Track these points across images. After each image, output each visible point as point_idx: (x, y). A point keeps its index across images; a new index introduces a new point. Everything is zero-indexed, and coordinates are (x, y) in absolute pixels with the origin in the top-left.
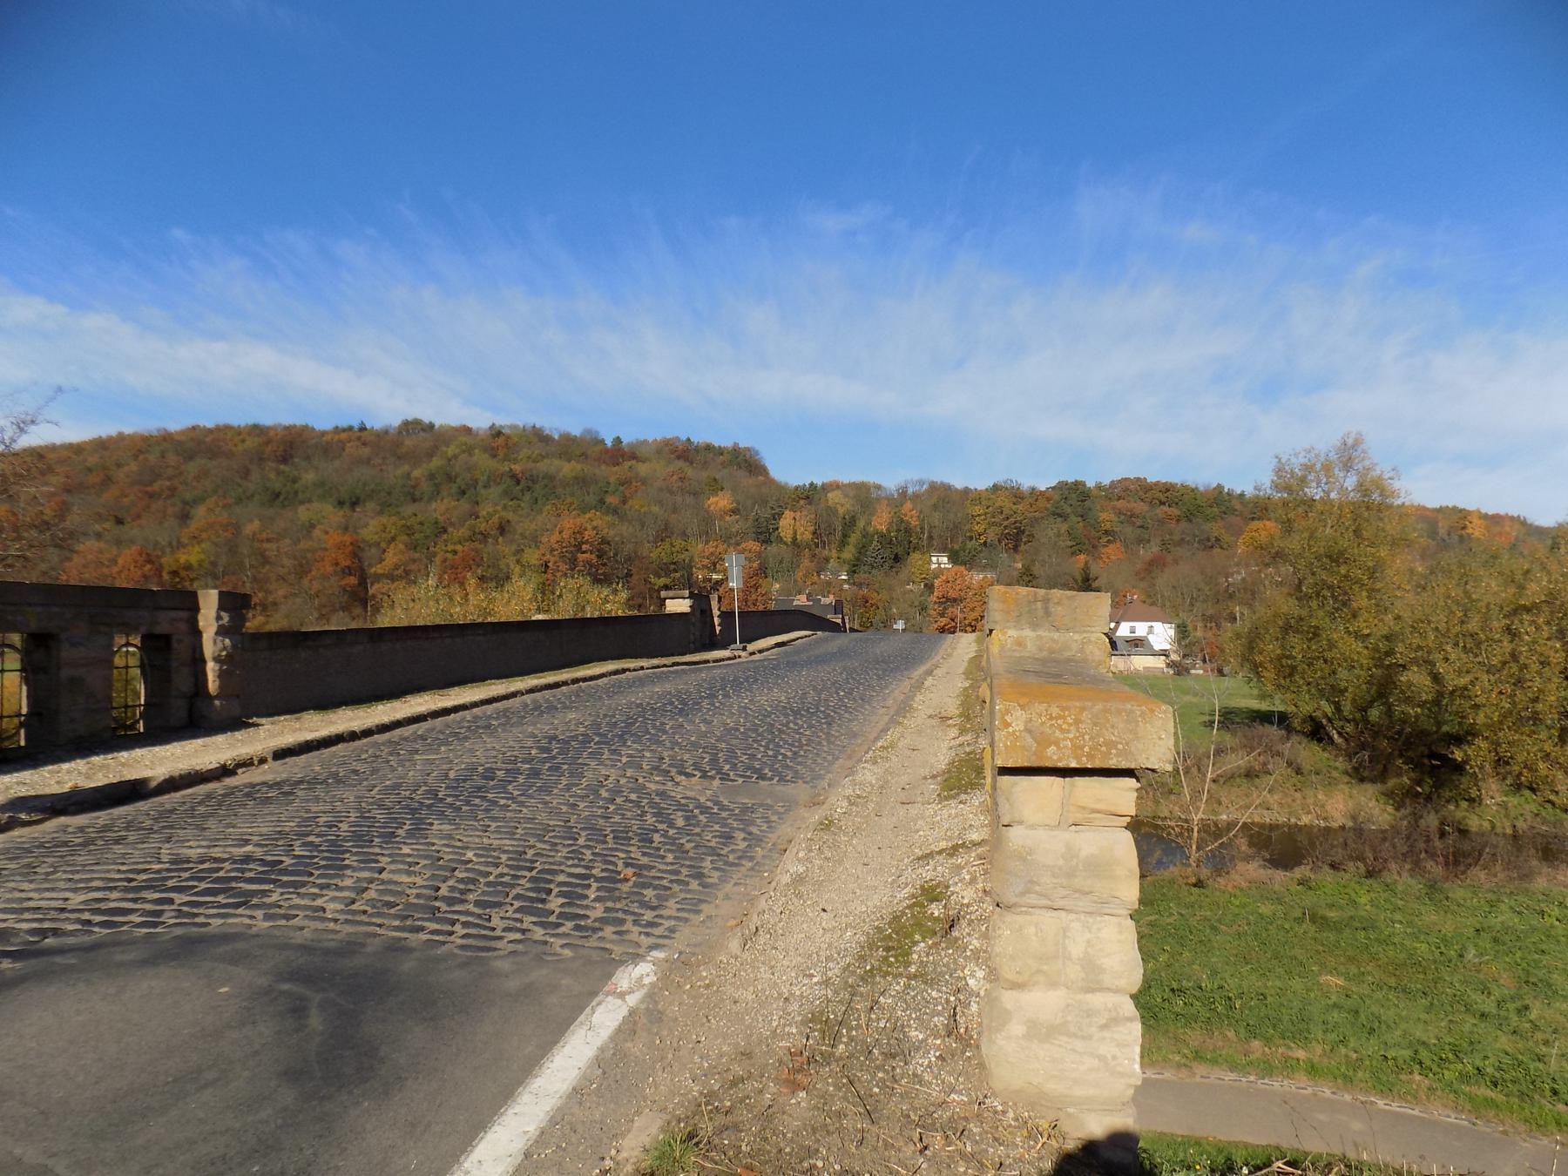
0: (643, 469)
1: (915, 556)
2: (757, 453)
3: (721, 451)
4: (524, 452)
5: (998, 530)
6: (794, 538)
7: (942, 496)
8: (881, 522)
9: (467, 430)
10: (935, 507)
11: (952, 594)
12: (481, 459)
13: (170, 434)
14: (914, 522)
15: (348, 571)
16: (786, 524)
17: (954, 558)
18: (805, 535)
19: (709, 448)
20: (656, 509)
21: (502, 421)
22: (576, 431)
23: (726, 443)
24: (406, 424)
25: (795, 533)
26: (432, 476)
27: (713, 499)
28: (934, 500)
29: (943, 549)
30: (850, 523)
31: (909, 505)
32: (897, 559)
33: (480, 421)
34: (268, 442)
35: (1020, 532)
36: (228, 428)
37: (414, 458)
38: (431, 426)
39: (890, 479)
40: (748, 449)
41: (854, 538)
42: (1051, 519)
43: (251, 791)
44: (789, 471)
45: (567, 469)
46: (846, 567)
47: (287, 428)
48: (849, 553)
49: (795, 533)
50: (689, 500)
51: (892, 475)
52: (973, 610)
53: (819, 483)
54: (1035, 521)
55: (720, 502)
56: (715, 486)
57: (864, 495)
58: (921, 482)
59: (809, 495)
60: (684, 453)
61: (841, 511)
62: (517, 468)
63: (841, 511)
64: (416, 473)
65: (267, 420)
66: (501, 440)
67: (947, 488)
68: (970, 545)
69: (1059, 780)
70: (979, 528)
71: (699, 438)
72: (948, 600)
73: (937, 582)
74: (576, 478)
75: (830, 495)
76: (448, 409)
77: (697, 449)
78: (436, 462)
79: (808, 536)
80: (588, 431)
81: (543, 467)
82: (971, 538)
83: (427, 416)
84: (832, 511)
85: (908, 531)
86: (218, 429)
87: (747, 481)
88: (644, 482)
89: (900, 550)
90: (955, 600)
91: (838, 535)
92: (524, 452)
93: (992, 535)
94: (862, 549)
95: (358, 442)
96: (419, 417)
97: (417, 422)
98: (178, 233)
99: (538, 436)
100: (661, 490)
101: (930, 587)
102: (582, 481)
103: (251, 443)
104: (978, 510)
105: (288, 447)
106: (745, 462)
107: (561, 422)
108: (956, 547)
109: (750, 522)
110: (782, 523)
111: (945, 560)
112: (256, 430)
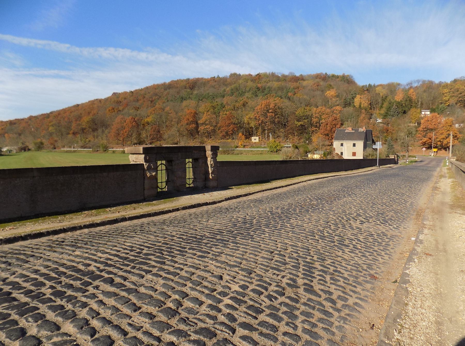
0: (305, 83)
1: (413, 110)
2: (352, 77)
3: (338, 77)
4: (264, 80)
5: (456, 99)
6: (360, 106)
7: (429, 86)
8: (399, 97)
10: (425, 91)
12: (250, 84)
14: (414, 97)
15: (192, 122)
16: (357, 101)
17: (433, 111)
18: (365, 104)
19: (333, 76)
20: (305, 97)
22: (286, 73)
25: (361, 103)
27: (328, 92)
28: (425, 88)
29: (428, 108)
30: (384, 99)
31: (412, 90)
32: (405, 112)
34: (188, 83)
39: (403, 80)
40: (348, 76)
41: (386, 105)
43: (220, 211)
44: (361, 81)
45: (275, 84)
46: (382, 117)
48: (383, 111)
49: (361, 103)
52: (442, 134)
53: (373, 84)
55: (330, 93)
56: (330, 87)
58: (418, 81)
59: (369, 89)
60: (325, 78)
61: (381, 94)
62: (259, 85)
63: (381, 94)
67: (431, 82)
68: (441, 106)
70: (446, 98)
71: (330, 73)
72: (428, 129)
73: (422, 121)
75: (377, 89)
77: (329, 77)
79: (366, 105)
80: (291, 73)
81: (268, 85)
82: (442, 103)
85: (410, 100)
86: (178, 80)
88: (304, 87)
89: (406, 109)
90: (432, 130)
91: (380, 105)
92: (264, 80)
93: (453, 101)
94: (389, 109)
95: (218, 82)
96: (393, 82)
101: (419, 124)
102: (281, 89)
103: (185, 83)
104: (446, 90)
105: (193, 85)
106: (347, 80)
108: (434, 107)
110: (356, 100)
111: (428, 113)
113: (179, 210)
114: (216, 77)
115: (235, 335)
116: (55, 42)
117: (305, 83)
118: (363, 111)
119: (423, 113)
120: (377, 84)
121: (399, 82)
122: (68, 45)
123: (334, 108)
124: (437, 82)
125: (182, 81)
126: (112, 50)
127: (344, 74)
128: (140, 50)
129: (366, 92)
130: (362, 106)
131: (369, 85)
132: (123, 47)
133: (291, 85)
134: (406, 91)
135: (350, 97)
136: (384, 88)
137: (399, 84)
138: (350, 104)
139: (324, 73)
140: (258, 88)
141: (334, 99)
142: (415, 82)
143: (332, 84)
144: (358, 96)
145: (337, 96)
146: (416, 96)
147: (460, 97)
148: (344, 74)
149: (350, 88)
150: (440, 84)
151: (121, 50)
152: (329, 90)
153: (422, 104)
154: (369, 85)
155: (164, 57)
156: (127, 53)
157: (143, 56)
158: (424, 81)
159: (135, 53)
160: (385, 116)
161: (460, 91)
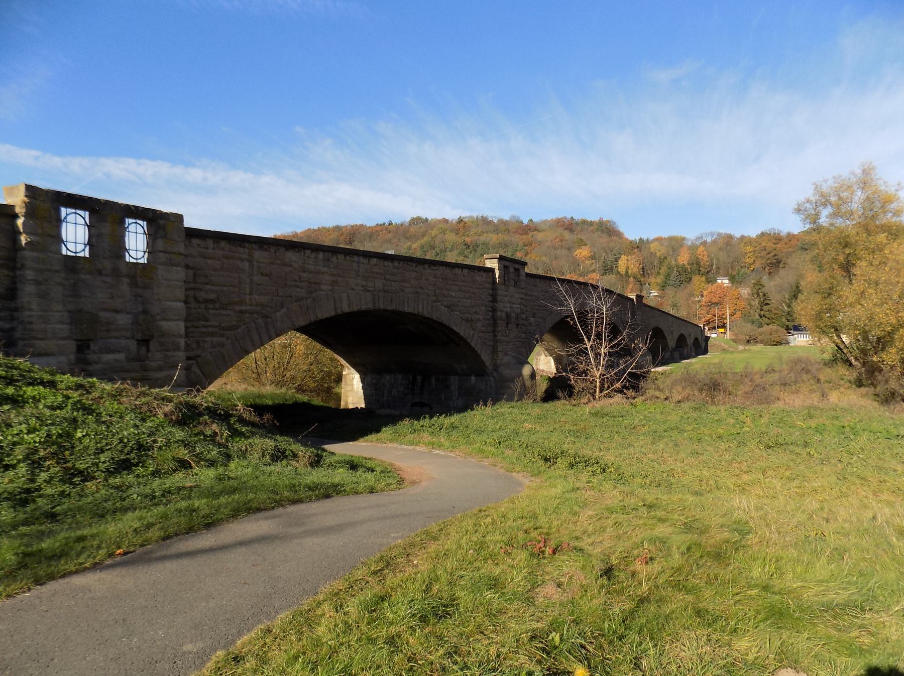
0: (540, 236)
2: (614, 223)
3: (592, 223)
4: (473, 231)
7: (727, 242)
8: (684, 259)
9: (446, 221)
11: (715, 300)
13: (794, 236)
16: (622, 264)
17: (732, 279)
18: (634, 269)
19: (584, 222)
20: (543, 258)
21: (465, 214)
22: (506, 217)
23: (594, 218)
24: (413, 219)
26: (422, 247)
33: (452, 215)
34: (342, 234)
35: (779, 262)
36: (324, 228)
37: (414, 238)
38: (427, 220)
39: (691, 233)
42: (799, 252)
44: (632, 233)
47: (352, 226)
50: (564, 252)
51: (693, 230)
53: (645, 238)
54: (789, 254)
55: (583, 253)
56: (581, 243)
57: (675, 244)
58: (712, 234)
59: (639, 246)
60: (570, 226)
62: (468, 240)
63: (658, 254)
64: (414, 246)
65: (343, 223)
66: (462, 224)
67: (730, 237)
69: (243, 550)
71: (578, 217)
74: (499, 243)
76: (433, 212)
77: (577, 224)
78: (426, 239)
80: (513, 217)
81: (482, 239)
83: (423, 215)
84: (653, 254)
85: (698, 264)
86: (319, 229)
87: (604, 240)
88: (540, 243)
97: (419, 218)
98: (298, 129)
99: (485, 221)
100: (548, 247)
104: (749, 249)
106: (607, 229)
107: (497, 213)
108: (734, 273)
109: (601, 263)
110: (620, 262)
111: (727, 281)
112: (337, 228)
113: (171, 537)
114: (387, 223)
115: (541, 404)
116: (8, 146)
117: (540, 236)
118: (631, 279)
119: (719, 281)
120: (651, 238)
121: (683, 235)
122: (34, 153)
123: (589, 276)
124: (738, 235)
125: (328, 230)
126: (131, 163)
127: (601, 220)
128: (188, 164)
129: (636, 250)
130: (630, 272)
131: (641, 239)
132: (153, 158)
133: (517, 239)
134: (693, 248)
135: (612, 258)
136: (662, 245)
137: (683, 239)
138: (612, 268)
139: (569, 217)
140: (467, 246)
141: (587, 262)
142: (707, 235)
143: (583, 237)
144: (624, 257)
145: (593, 257)
146: (708, 256)
147: (768, 259)
148: (601, 220)
149: (612, 244)
150: (743, 237)
151: (149, 162)
152: (579, 247)
153: (718, 268)
154: (641, 239)
155: (238, 177)
156: (164, 169)
157: (195, 174)
158: (719, 234)
159: (179, 170)
160: (663, 287)
161: (768, 249)
